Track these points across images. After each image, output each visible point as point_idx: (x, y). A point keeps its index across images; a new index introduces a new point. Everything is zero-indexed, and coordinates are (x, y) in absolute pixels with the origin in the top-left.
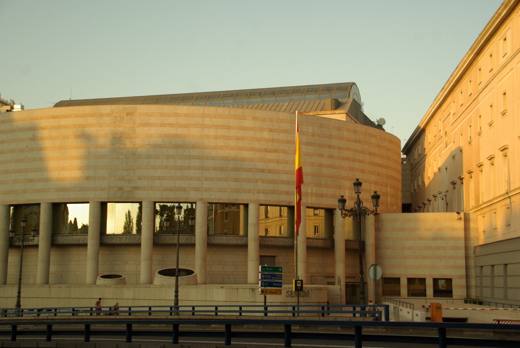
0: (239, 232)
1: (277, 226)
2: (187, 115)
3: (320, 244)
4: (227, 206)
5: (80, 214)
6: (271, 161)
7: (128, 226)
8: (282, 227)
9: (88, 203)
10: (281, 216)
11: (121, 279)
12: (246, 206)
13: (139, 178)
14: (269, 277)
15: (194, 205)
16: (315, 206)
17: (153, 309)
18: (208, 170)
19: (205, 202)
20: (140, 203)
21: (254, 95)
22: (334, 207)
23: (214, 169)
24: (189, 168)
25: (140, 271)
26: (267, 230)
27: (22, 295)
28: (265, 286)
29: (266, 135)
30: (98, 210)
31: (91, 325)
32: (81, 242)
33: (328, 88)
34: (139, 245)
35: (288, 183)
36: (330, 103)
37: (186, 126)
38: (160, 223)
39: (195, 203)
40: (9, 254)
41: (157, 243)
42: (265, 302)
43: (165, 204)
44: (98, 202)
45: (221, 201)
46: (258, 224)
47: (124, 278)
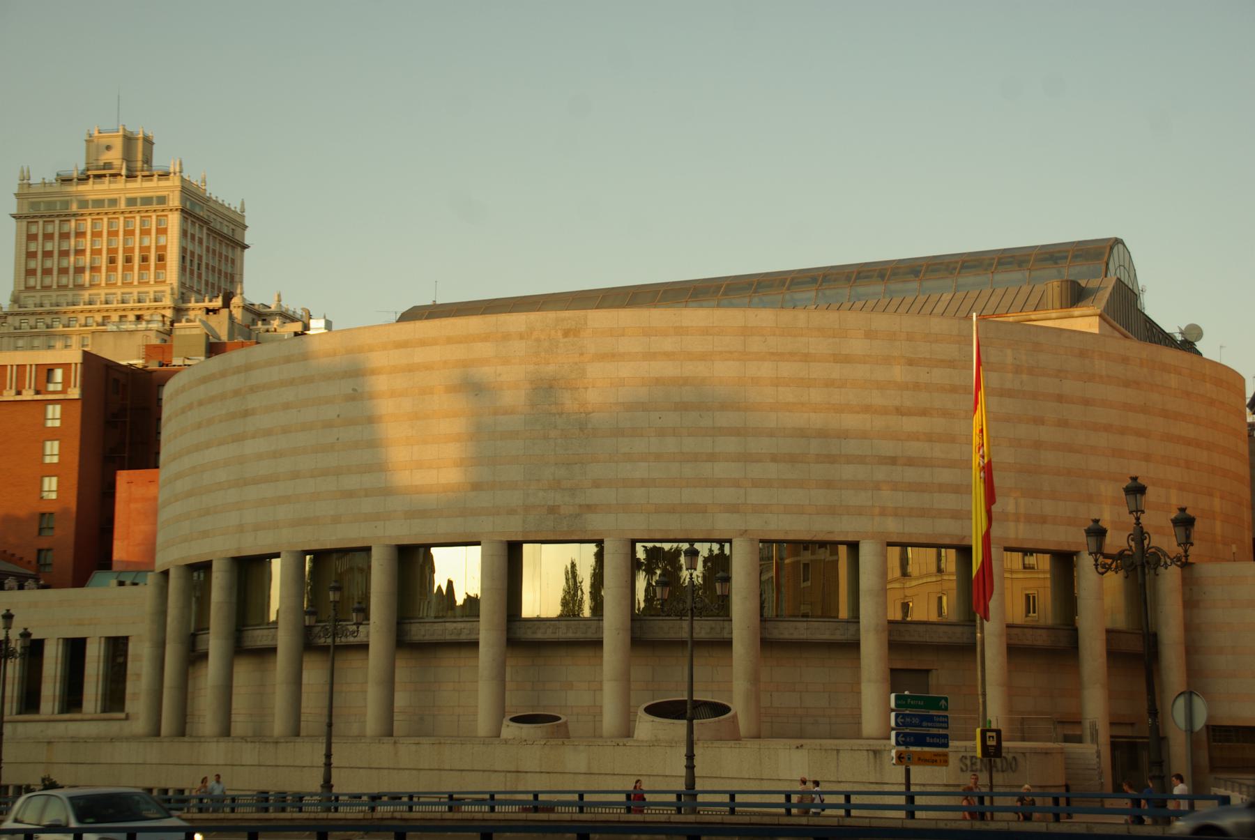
1: (930, 596)
2: (705, 332)
3: (1041, 639)
4: (806, 549)
5: (459, 570)
7: (571, 600)
8: (945, 599)
9: (478, 544)
10: (940, 570)
11: (558, 726)
12: (854, 547)
13: (597, 484)
15: (727, 546)
19: (752, 540)
20: (599, 543)
21: (867, 277)
22: (1073, 549)
24: (712, 458)
26: (905, 607)
27: (335, 761)
28: (906, 744)
29: (898, 373)
30: (501, 562)
32: (464, 637)
34: (598, 644)
36: (1057, 290)
37: (704, 357)
38: (647, 590)
39: (730, 541)
41: (641, 639)
43: (658, 545)
44: (501, 542)
46: (883, 591)
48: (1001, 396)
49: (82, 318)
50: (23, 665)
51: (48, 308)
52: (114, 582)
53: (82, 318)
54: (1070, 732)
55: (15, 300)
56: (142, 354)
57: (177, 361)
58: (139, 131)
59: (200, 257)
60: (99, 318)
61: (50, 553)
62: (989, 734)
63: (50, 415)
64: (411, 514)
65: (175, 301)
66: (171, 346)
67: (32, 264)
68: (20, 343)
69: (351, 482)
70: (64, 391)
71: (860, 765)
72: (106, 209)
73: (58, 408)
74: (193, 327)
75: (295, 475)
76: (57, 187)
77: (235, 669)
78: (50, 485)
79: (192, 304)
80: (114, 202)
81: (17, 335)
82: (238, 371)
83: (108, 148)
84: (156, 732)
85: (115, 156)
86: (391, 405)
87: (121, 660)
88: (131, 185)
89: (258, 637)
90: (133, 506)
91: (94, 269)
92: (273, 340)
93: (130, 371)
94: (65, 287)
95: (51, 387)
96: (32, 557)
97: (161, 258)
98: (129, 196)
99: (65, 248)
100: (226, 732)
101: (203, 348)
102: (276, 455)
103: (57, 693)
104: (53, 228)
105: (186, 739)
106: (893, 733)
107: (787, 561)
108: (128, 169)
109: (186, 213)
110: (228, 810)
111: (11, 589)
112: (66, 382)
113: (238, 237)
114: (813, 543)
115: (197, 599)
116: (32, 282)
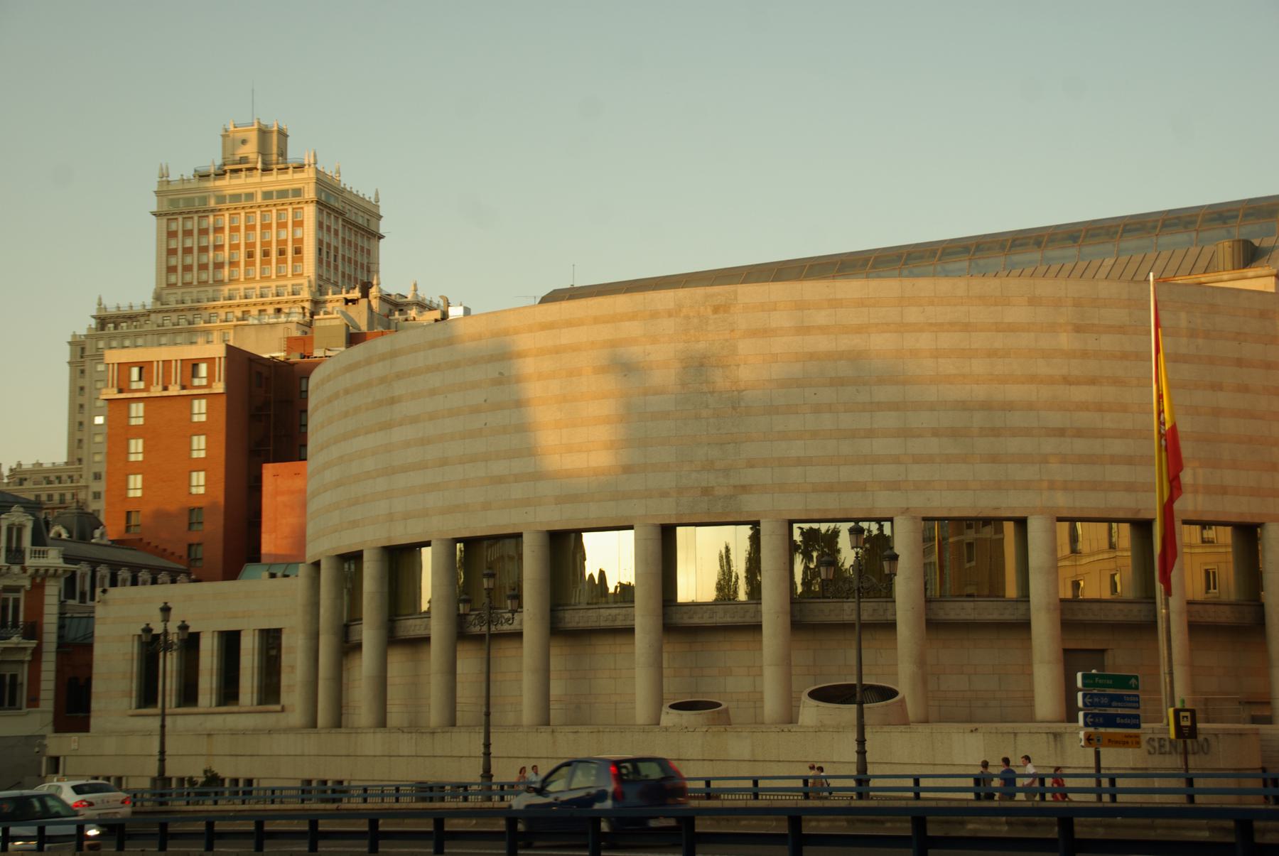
0: (1004, 589)
1: (1103, 570)
2: (861, 303)
3: (1224, 616)
4: (969, 527)
5: (612, 557)
6: (1083, 407)
7: (725, 585)
8: (1117, 578)
9: (631, 528)
10: (1112, 546)
11: (719, 712)
12: (1021, 523)
13: (751, 464)
14: (1105, 701)
15: (887, 526)
17: (762, 784)
18: (919, 436)
19: (915, 518)
20: (755, 525)
21: (1021, 245)
22: (1257, 520)
23: (936, 433)
24: (870, 434)
25: (762, 693)
26: (1076, 585)
27: (168, 751)
28: (1095, 725)
29: (1065, 340)
30: (655, 546)
31: (266, 822)
32: (619, 624)
33: (1220, 215)
34: (757, 628)
36: (1228, 251)
37: (860, 329)
38: (805, 573)
39: (891, 520)
40: (459, 655)
41: (801, 623)
42: (1187, 769)
43: (815, 526)
44: (655, 525)
45: (955, 514)
46: (1054, 569)
47: (726, 710)
49: (222, 313)
50: (180, 658)
51: (189, 304)
52: (266, 574)
53: (222, 313)
54: (1258, 713)
55: (158, 297)
56: (284, 346)
57: (318, 353)
58: (273, 123)
59: (336, 249)
60: (239, 313)
61: (200, 548)
62: (1182, 714)
63: (196, 410)
64: (561, 500)
65: (312, 293)
66: (312, 338)
67: (173, 262)
68: (164, 340)
69: (499, 468)
70: (209, 386)
71: (1050, 747)
72: (243, 203)
73: (141, 405)
74: (334, 315)
75: (444, 462)
76: (195, 184)
77: (389, 660)
78: (199, 479)
79: (330, 297)
80: (250, 196)
81: (160, 332)
82: (383, 358)
83: (244, 142)
84: (314, 724)
85: (250, 150)
86: (540, 388)
87: (273, 652)
88: (267, 179)
89: (411, 627)
90: (279, 499)
91: (233, 264)
92: (412, 327)
93: (272, 364)
94: (205, 283)
95: (196, 382)
96: (184, 553)
97: (298, 251)
98: (265, 189)
99: (204, 243)
100: (382, 722)
101: (343, 339)
102: (424, 442)
103: (214, 686)
104: (192, 225)
105: (343, 730)
106: (1081, 714)
107: (951, 540)
108: (264, 163)
109: (321, 205)
110: (496, 798)
111: (144, 583)
112: (210, 377)
113: (373, 228)
114: (977, 519)
115: (349, 590)
116: (173, 279)
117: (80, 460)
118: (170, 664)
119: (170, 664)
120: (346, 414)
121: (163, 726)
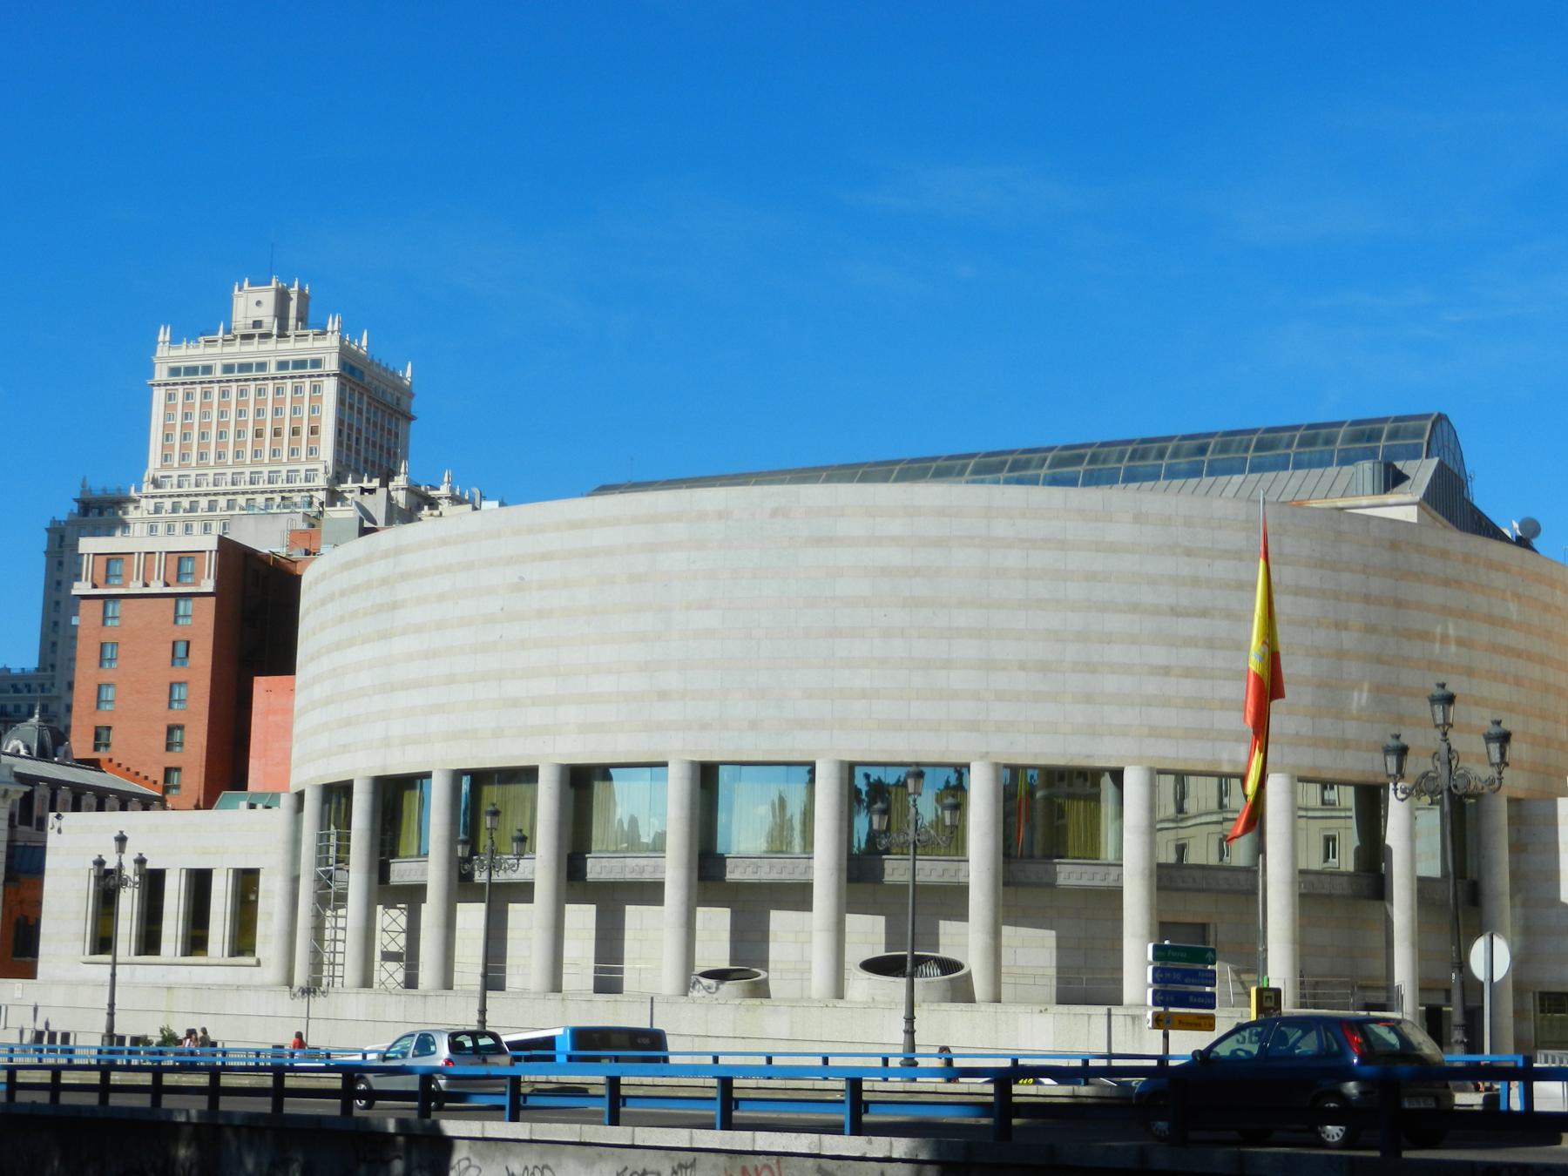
12: (1117, 776)
14: (1177, 976)
16: (1327, 775)
35: (1225, 705)
36: (1368, 474)
44: (693, 763)
48: (1296, 594)
52: (244, 804)
56: (286, 541)
59: (359, 431)
82: (385, 555)
84: (289, 982)
88: (282, 346)
89: (402, 872)
108: (279, 328)
117: (53, 666)
118: (128, 903)
119: (128, 903)
120: (342, 619)
121: (113, 975)
